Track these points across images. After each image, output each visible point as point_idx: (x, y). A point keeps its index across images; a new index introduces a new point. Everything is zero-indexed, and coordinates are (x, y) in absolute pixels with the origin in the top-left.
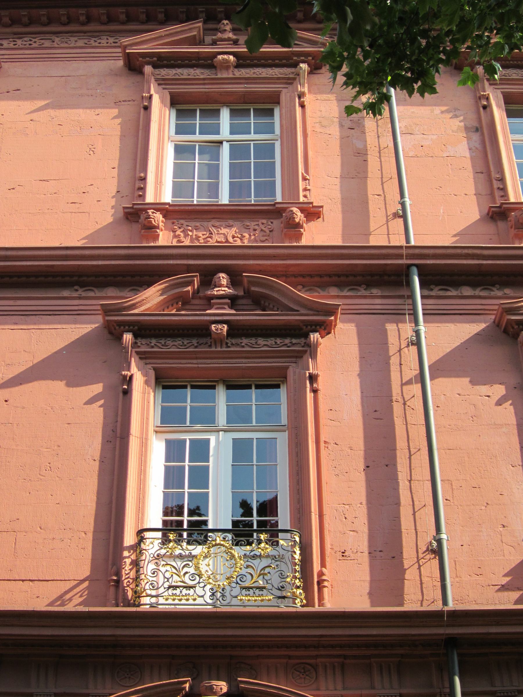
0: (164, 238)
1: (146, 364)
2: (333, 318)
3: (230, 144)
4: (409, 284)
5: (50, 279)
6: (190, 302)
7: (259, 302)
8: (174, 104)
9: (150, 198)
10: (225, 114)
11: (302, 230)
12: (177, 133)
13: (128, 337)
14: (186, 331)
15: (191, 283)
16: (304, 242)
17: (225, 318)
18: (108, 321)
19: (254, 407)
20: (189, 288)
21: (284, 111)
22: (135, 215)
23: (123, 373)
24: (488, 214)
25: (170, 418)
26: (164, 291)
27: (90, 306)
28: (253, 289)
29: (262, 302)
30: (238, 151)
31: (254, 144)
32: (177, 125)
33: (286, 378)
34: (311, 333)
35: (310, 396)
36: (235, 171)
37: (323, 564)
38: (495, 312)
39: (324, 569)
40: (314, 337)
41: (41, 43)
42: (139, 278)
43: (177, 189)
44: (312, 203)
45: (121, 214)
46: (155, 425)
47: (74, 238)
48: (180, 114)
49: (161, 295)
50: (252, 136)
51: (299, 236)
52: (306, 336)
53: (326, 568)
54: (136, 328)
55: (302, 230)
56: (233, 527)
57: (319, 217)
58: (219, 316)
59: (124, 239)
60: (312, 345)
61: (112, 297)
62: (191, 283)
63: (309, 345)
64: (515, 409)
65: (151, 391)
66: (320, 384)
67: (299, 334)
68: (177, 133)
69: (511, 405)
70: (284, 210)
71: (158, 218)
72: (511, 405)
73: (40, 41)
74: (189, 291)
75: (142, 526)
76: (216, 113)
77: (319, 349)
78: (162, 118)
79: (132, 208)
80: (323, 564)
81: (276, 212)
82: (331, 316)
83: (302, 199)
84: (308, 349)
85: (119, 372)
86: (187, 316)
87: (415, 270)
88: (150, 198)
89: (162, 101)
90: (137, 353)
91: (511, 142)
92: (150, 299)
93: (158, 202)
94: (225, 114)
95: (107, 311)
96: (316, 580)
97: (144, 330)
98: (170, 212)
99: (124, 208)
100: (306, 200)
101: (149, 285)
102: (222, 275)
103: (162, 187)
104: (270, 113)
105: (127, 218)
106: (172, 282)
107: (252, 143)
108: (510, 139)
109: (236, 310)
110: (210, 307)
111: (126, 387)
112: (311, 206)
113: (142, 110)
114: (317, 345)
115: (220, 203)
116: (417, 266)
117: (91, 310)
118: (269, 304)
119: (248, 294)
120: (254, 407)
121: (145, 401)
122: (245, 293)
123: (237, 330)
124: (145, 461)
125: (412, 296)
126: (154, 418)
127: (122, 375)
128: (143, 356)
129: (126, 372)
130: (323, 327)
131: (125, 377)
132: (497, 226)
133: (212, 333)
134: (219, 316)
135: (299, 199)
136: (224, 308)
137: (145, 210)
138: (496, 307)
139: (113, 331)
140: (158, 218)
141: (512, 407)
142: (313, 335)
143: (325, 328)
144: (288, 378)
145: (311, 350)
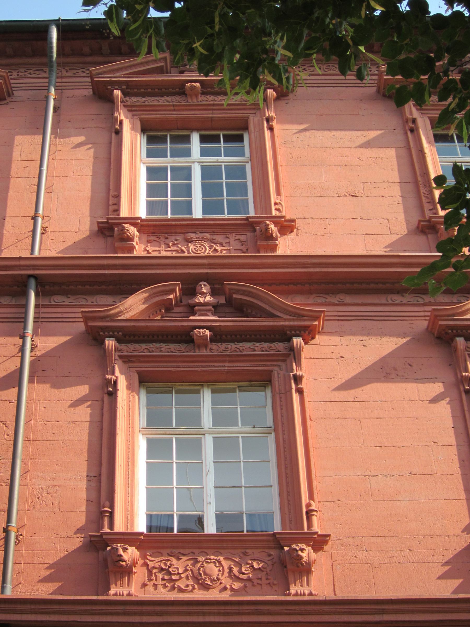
0: (139, 249)
1: (129, 367)
2: (316, 323)
3: (201, 166)
4: (25, 295)
5: (364, 286)
6: (173, 309)
7: (240, 309)
8: (144, 130)
9: (124, 213)
10: (195, 138)
11: (134, 243)
12: (148, 156)
13: (110, 343)
14: (146, 337)
15: (173, 291)
16: (279, 252)
17: (210, 324)
18: (92, 327)
19: (174, 409)
20: (172, 296)
21: (253, 135)
22: (109, 229)
23: (107, 377)
24: (418, 228)
25: (154, 420)
26: (146, 300)
27: (60, 314)
28: (235, 296)
29: (245, 310)
30: (207, 172)
31: (225, 165)
32: (148, 150)
33: (270, 381)
34: (106, 339)
35: (296, 397)
36: (207, 190)
37: (311, 497)
38: (428, 318)
39: (312, 502)
40: (297, 341)
41: (312, 70)
42: (124, 286)
43: (151, 207)
44: (283, 217)
45: (96, 228)
46: (141, 427)
47: (378, 248)
48: (151, 140)
49: (144, 303)
50: (223, 158)
51: (274, 248)
52: (289, 340)
53: (314, 502)
54: (120, 333)
55: (277, 242)
56: (217, 531)
57: (292, 231)
58: (204, 322)
59: (98, 252)
60: (296, 350)
61: (99, 304)
62: (173, 291)
63: (292, 349)
64: (451, 407)
65: (136, 395)
66: (304, 385)
67: (284, 339)
68: (148, 156)
69: (448, 404)
70: (258, 223)
71: (130, 554)
72: (448, 404)
73: (310, 68)
74: (171, 299)
75: (134, 214)
76: (187, 139)
77: (302, 353)
78: (133, 142)
79: (107, 223)
80: (311, 497)
81: (250, 225)
82: (316, 321)
83: (274, 213)
84: (292, 353)
85: (104, 376)
86: (176, 322)
87: (32, 283)
88: (124, 213)
89: (133, 129)
90: (120, 357)
91: (439, 163)
92: (133, 307)
93: (129, 531)
94: (195, 138)
95: (87, 318)
96: (304, 510)
97: (129, 335)
98: (142, 226)
99: (99, 223)
100: (278, 214)
101: (132, 292)
102: (202, 283)
103: (137, 203)
104: (240, 139)
105: (102, 233)
106: (155, 291)
107: (223, 164)
108: (438, 160)
109: (218, 317)
110: (194, 314)
111: (111, 389)
112: (283, 219)
113: (113, 135)
114: (300, 350)
115: (194, 217)
116: (35, 277)
117: (365, 316)
118: (252, 311)
119: (230, 302)
120: (174, 409)
121: (131, 406)
122: (226, 302)
123: (219, 336)
124: (133, 460)
125: (26, 306)
126: (141, 420)
127: (106, 379)
128: (127, 360)
129: (110, 376)
130: (307, 332)
131: (109, 381)
132: (427, 237)
133: (195, 337)
134: (204, 322)
135: (271, 213)
136: (208, 315)
137: (120, 224)
138: (429, 314)
139: (94, 338)
140: (133, 231)
141: (449, 406)
142: (109, 341)
143: (309, 334)
144: (273, 381)
145: (294, 355)
